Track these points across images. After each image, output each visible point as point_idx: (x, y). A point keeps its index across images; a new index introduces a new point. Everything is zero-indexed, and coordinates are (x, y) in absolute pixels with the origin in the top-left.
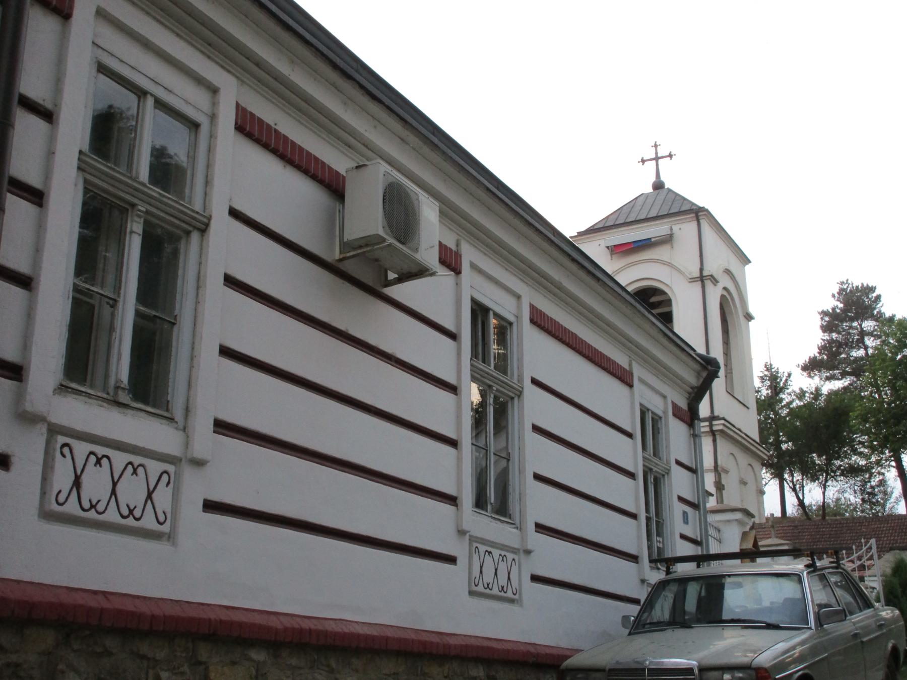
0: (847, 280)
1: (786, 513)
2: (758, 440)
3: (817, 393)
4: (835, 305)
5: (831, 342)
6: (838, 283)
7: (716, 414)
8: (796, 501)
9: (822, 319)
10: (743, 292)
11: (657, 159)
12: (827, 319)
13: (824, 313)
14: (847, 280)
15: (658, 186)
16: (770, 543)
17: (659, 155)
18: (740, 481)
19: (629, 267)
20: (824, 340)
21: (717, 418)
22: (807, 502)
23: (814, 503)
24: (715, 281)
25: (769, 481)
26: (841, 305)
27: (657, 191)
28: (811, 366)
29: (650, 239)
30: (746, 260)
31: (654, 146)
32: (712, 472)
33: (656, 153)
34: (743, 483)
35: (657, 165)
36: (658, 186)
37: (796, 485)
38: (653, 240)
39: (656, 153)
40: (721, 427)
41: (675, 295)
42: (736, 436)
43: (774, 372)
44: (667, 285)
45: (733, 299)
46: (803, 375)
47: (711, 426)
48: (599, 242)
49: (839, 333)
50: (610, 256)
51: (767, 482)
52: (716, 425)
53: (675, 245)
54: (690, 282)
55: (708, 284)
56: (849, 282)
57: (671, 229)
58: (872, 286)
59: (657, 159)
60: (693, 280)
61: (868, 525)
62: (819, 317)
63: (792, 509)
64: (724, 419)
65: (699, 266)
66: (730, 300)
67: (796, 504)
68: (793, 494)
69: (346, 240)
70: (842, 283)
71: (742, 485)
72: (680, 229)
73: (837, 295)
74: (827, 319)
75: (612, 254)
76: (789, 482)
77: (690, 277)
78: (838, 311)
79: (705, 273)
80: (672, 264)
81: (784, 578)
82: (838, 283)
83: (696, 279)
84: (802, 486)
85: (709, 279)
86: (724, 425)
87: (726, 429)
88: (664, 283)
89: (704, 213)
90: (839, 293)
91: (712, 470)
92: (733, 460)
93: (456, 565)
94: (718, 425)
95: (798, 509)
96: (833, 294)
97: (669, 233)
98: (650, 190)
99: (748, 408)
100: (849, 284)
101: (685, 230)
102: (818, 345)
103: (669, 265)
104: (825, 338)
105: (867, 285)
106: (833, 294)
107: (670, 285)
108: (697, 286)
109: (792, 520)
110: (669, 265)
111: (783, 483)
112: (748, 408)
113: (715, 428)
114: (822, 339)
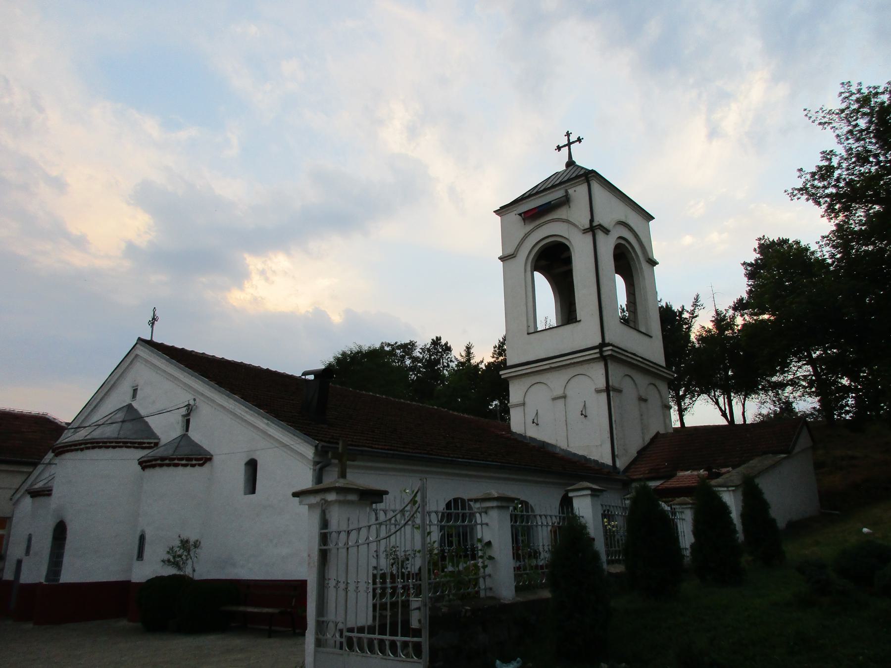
0: (764, 236)
2: (664, 365)
6: (756, 240)
7: (607, 341)
11: (569, 144)
14: (764, 236)
15: (570, 163)
18: (639, 398)
19: (537, 228)
20: (749, 285)
21: (609, 345)
24: (606, 231)
29: (550, 202)
32: (604, 392)
33: (569, 140)
34: (643, 400)
35: (570, 149)
36: (570, 163)
38: (552, 203)
39: (569, 140)
40: (610, 353)
41: (571, 243)
47: (601, 352)
53: (571, 205)
54: (584, 233)
55: (600, 235)
56: (766, 237)
57: (566, 192)
58: (786, 239)
59: (569, 144)
60: (585, 231)
62: (742, 268)
65: (589, 217)
66: (627, 245)
69: (712, 324)
70: (760, 239)
72: (575, 191)
75: (524, 220)
77: (583, 228)
79: (595, 224)
80: (569, 221)
81: (506, 496)
82: (756, 240)
83: (588, 230)
85: (599, 228)
86: (612, 350)
87: (615, 354)
88: (565, 237)
89: (592, 175)
90: (759, 247)
92: (630, 379)
93: (245, 494)
94: (607, 351)
98: (564, 168)
99: (651, 337)
101: (579, 193)
103: (567, 221)
104: (750, 283)
105: (783, 238)
108: (589, 238)
110: (567, 221)
112: (651, 337)
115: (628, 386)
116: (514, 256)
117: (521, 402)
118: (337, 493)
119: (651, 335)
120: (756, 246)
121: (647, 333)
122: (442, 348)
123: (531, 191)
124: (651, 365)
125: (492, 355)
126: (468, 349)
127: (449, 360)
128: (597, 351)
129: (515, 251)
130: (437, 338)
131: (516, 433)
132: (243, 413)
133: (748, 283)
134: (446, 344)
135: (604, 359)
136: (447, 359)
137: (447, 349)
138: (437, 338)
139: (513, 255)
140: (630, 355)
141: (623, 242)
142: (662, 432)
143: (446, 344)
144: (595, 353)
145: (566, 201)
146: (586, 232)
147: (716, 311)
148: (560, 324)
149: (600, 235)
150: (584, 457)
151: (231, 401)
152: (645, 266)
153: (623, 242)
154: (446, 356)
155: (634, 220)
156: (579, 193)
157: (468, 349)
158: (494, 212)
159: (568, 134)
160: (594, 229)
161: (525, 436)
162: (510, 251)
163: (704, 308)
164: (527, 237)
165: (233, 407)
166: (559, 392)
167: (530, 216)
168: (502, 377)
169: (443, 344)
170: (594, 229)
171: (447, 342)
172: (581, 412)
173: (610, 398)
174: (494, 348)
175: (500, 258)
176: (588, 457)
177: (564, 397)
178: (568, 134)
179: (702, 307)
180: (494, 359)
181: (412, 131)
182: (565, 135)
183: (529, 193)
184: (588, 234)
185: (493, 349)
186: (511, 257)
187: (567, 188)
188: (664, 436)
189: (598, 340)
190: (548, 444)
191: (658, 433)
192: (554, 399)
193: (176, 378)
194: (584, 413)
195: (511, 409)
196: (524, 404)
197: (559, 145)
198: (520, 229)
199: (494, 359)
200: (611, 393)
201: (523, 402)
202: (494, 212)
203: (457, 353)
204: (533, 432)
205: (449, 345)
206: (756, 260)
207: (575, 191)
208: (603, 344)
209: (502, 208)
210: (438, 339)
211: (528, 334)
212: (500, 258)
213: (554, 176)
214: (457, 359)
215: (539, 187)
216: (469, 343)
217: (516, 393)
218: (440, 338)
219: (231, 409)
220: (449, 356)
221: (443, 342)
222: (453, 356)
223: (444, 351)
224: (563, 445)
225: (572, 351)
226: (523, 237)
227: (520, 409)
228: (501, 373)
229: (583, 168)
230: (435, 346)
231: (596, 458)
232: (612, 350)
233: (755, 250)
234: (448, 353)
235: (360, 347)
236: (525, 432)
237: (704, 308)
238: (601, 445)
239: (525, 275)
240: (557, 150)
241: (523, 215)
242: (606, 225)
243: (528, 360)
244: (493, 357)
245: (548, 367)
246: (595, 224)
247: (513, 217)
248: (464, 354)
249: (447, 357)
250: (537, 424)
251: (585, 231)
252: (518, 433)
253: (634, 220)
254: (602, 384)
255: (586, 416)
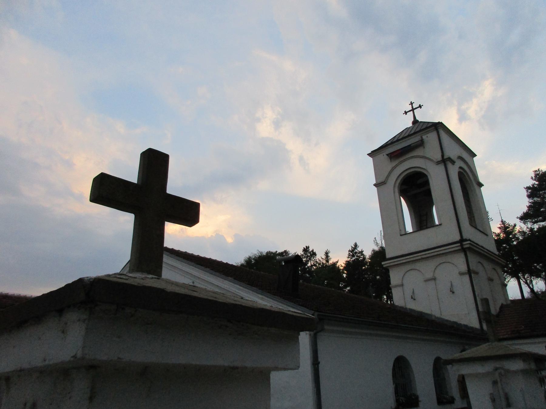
0: (539, 169)
1: (524, 297)
3: (531, 230)
4: (534, 183)
5: (534, 203)
7: (464, 237)
8: (529, 290)
9: (527, 191)
10: (474, 170)
11: (413, 110)
12: (530, 191)
13: (528, 188)
14: (539, 169)
15: (415, 122)
16: (485, 354)
17: (414, 108)
20: (530, 202)
21: (466, 240)
22: (535, 289)
23: (539, 290)
24: (453, 162)
25: (510, 279)
26: (537, 183)
27: (414, 125)
28: (524, 218)
30: (475, 155)
31: (412, 103)
32: (467, 274)
33: (412, 107)
34: (491, 280)
35: (414, 113)
37: (527, 280)
39: (412, 107)
40: (468, 246)
42: (480, 251)
43: (507, 225)
44: (424, 169)
45: (465, 171)
46: (521, 222)
47: (462, 245)
48: (383, 154)
49: (538, 197)
50: (389, 160)
51: (509, 280)
52: (465, 244)
54: (437, 164)
55: (450, 165)
57: (422, 138)
59: (413, 110)
60: (438, 163)
61: (286, 254)
63: (527, 294)
64: (469, 240)
66: (465, 174)
67: (529, 292)
68: (526, 285)
70: (536, 171)
71: (490, 282)
72: (427, 137)
73: (533, 177)
74: (530, 191)
76: (522, 278)
77: (437, 161)
78: (535, 186)
79: (445, 157)
83: (441, 162)
84: (531, 281)
85: (448, 160)
91: (467, 273)
94: (466, 245)
95: (531, 294)
96: (532, 177)
97: (421, 139)
100: (540, 171)
101: (431, 138)
102: (527, 206)
104: (530, 201)
106: (532, 177)
107: (425, 168)
108: (442, 167)
109: (528, 300)
111: (520, 280)
113: (465, 246)
114: (529, 202)
115: (479, 269)
116: (384, 183)
117: (399, 284)
118: (524, 361)
119: (487, 234)
120: (533, 176)
121: (484, 232)
122: (310, 253)
123: (392, 140)
124: (491, 253)
125: (347, 256)
126: (327, 254)
127: (315, 261)
128: (459, 244)
129: (385, 179)
130: (306, 247)
131: (398, 306)
132: (237, 291)
133: (529, 201)
134: (313, 251)
135: (464, 250)
136: (314, 261)
137: (314, 254)
138: (306, 247)
139: (384, 182)
140: (480, 247)
141: (462, 171)
142: (505, 303)
143: (313, 251)
144: (457, 247)
145: (421, 144)
146: (439, 164)
147: (503, 222)
148: (415, 230)
149: (450, 165)
150: (455, 323)
151: (226, 282)
152: (476, 186)
153: (462, 171)
154: (313, 258)
155: (465, 155)
156: (431, 138)
157: (327, 254)
158: (368, 154)
159: (412, 104)
160: (445, 161)
161: (406, 308)
162: (382, 179)
163: (492, 220)
164: (393, 170)
165: (228, 287)
166: (429, 275)
167: (393, 156)
168: (384, 266)
169: (311, 251)
170: (445, 161)
171: (313, 249)
172: (450, 290)
173: (472, 279)
174: (349, 251)
175: (375, 185)
176: (458, 322)
177: (434, 279)
178: (412, 104)
179: (491, 220)
180: (349, 259)
181: (277, 124)
182: (410, 104)
183: (391, 140)
184: (440, 165)
185: (348, 252)
186: (383, 183)
187: (422, 135)
188: (507, 306)
189: (458, 238)
190: (424, 313)
191: (502, 304)
192: (427, 281)
193: (175, 267)
194: (452, 290)
195: (392, 289)
196: (402, 285)
197: (405, 111)
198: (388, 165)
199: (349, 259)
200: (473, 275)
201: (401, 284)
202: (368, 154)
203: (320, 256)
204: (411, 305)
205: (314, 251)
206: (533, 185)
207: (427, 137)
208: (462, 240)
209: (373, 152)
210: (308, 248)
211: (401, 235)
212: (375, 185)
213: (406, 130)
214: (320, 260)
215: (403, 134)
216: (327, 250)
217: (395, 277)
218: (309, 247)
219: (226, 288)
220: (315, 259)
221: (311, 249)
222: (318, 259)
223: (311, 255)
224: (438, 315)
225: (437, 246)
226: (392, 169)
227: (400, 289)
228: (383, 263)
229: (429, 123)
230: (305, 252)
231: (465, 323)
232: (470, 244)
233: (532, 178)
234: (314, 257)
235: (261, 253)
236: (405, 305)
237: (492, 220)
238: (469, 313)
239: (394, 195)
240: (405, 114)
241: (389, 155)
242: (452, 157)
243: (403, 254)
244: (348, 257)
245: (420, 257)
246: (445, 157)
247: (383, 157)
248: (324, 257)
249: (314, 259)
250: (414, 299)
251: (438, 163)
252: (400, 306)
253: (465, 155)
254: (464, 268)
255: (453, 293)
